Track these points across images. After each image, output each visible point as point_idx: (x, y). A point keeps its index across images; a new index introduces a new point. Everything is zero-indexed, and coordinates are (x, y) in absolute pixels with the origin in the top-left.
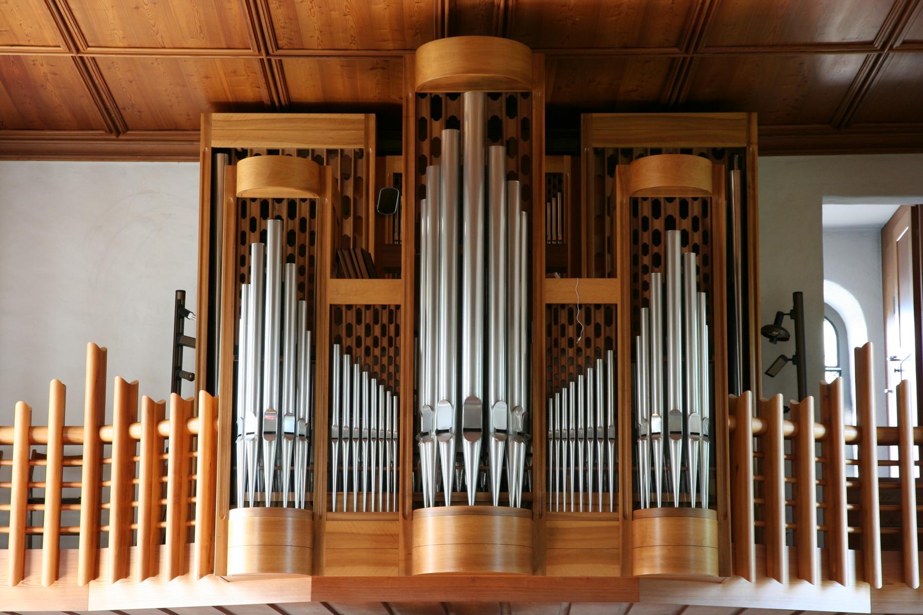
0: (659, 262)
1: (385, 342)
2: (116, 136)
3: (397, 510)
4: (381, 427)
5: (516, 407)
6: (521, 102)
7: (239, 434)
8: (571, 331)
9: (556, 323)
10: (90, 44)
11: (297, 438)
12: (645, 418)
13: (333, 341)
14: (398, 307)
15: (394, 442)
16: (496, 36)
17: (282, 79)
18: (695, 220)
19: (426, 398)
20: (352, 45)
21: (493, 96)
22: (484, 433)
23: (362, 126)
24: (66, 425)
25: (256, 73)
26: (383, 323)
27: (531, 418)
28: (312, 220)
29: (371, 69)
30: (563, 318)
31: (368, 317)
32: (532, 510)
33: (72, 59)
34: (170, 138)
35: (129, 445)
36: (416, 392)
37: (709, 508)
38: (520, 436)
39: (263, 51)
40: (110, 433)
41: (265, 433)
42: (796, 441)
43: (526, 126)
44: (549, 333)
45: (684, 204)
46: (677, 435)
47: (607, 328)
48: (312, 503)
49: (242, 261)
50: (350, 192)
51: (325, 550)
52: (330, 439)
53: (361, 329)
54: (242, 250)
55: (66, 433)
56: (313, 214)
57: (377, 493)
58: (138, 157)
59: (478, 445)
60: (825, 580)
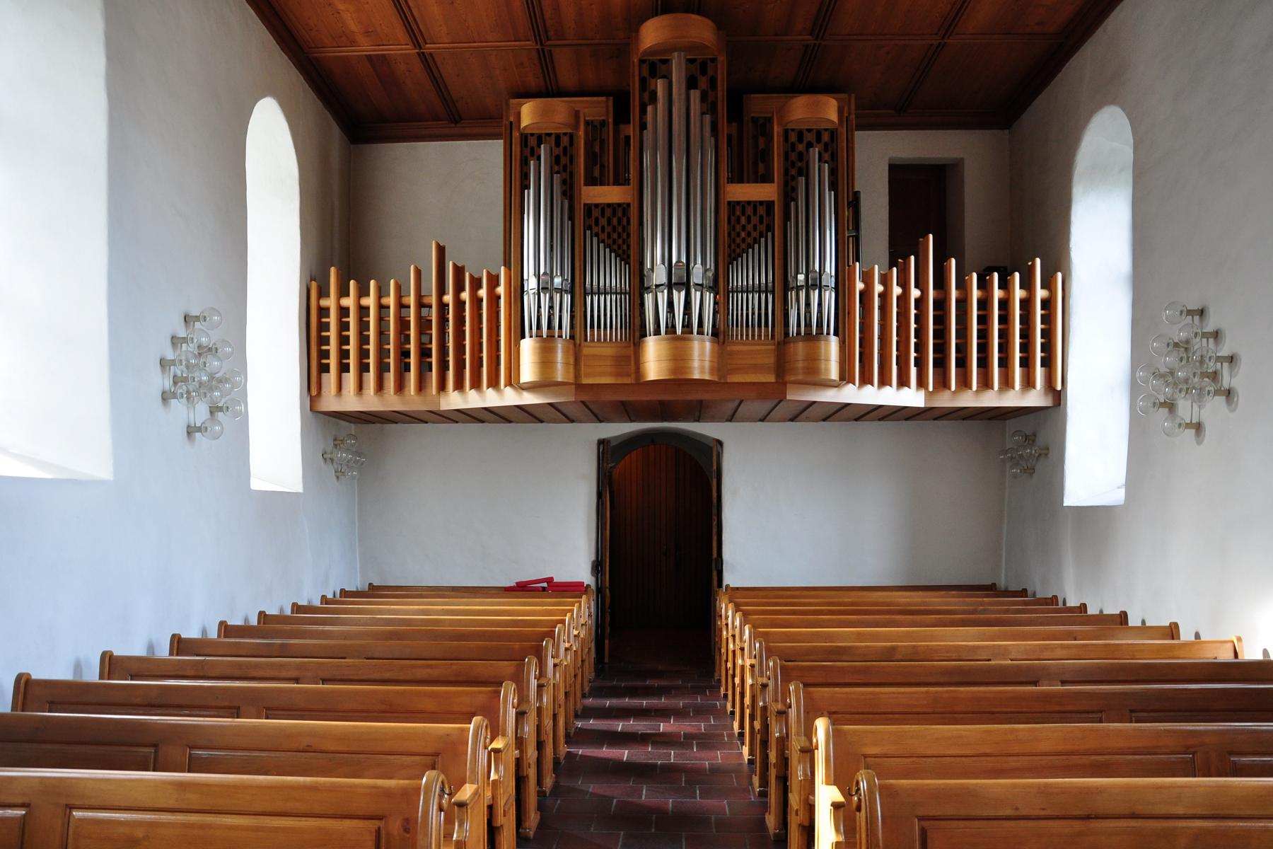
0: (805, 172)
1: (620, 229)
3: (630, 340)
9: (734, 214)
10: (428, 41)
14: (629, 205)
16: (693, 13)
18: (826, 144)
21: (691, 61)
22: (686, 285)
31: (608, 212)
35: (460, 304)
38: (711, 289)
39: (539, 43)
40: (449, 298)
42: (884, 296)
43: (713, 82)
44: (729, 222)
45: (819, 134)
50: (597, 149)
51: (583, 367)
52: (585, 294)
56: (571, 143)
59: (683, 293)
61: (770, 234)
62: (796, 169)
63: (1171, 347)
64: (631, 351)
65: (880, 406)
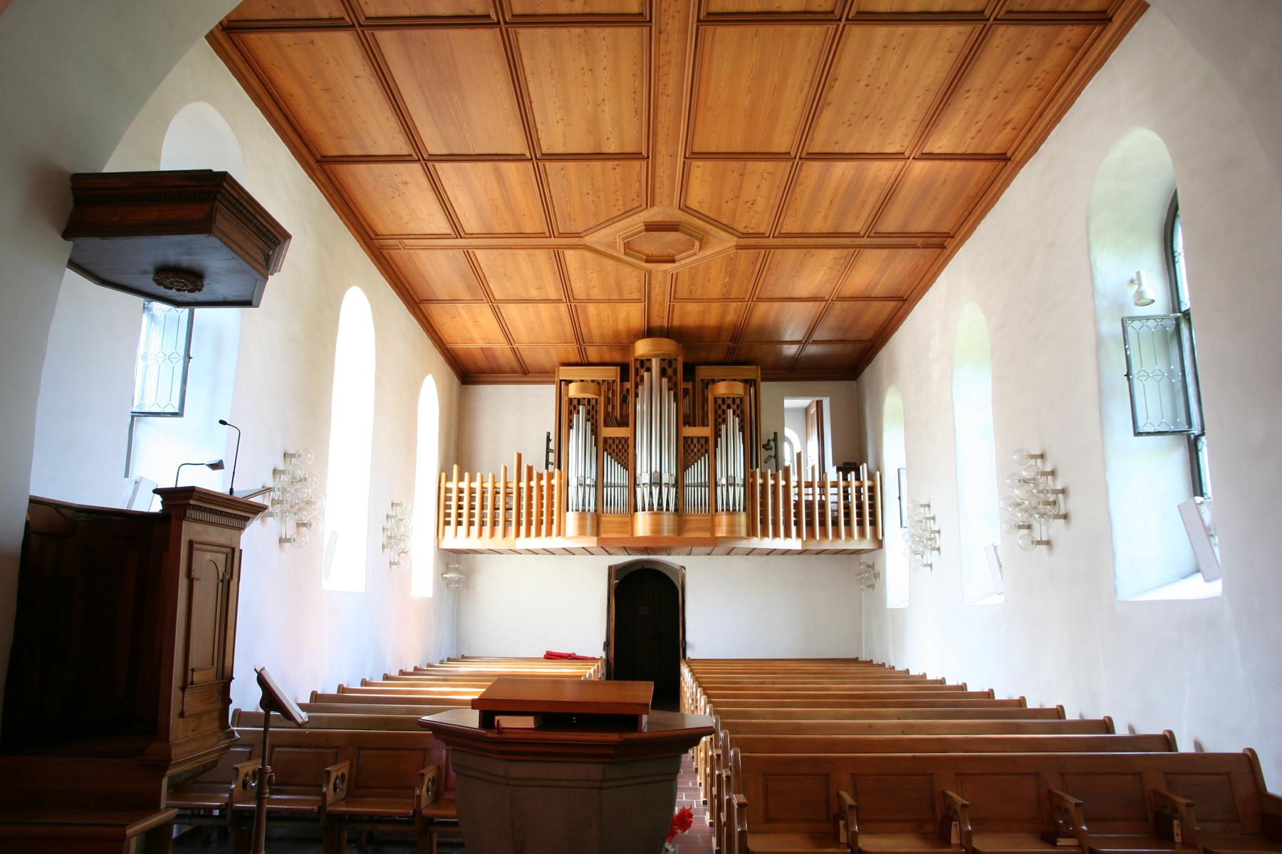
0: (725, 421)
1: (623, 451)
9: (687, 443)
14: (628, 438)
18: (738, 405)
31: (617, 442)
35: (530, 489)
36: (635, 469)
38: (673, 485)
40: (523, 484)
42: (775, 487)
43: (675, 371)
44: (684, 448)
45: (734, 400)
49: (571, 421)
50: (610, 396)
52: (603, 487)
59: (658, 489)
61: (707, 455)
62: (721, 420)
63: (1022, 483)
64: (628, 519)
65: (775, 549)
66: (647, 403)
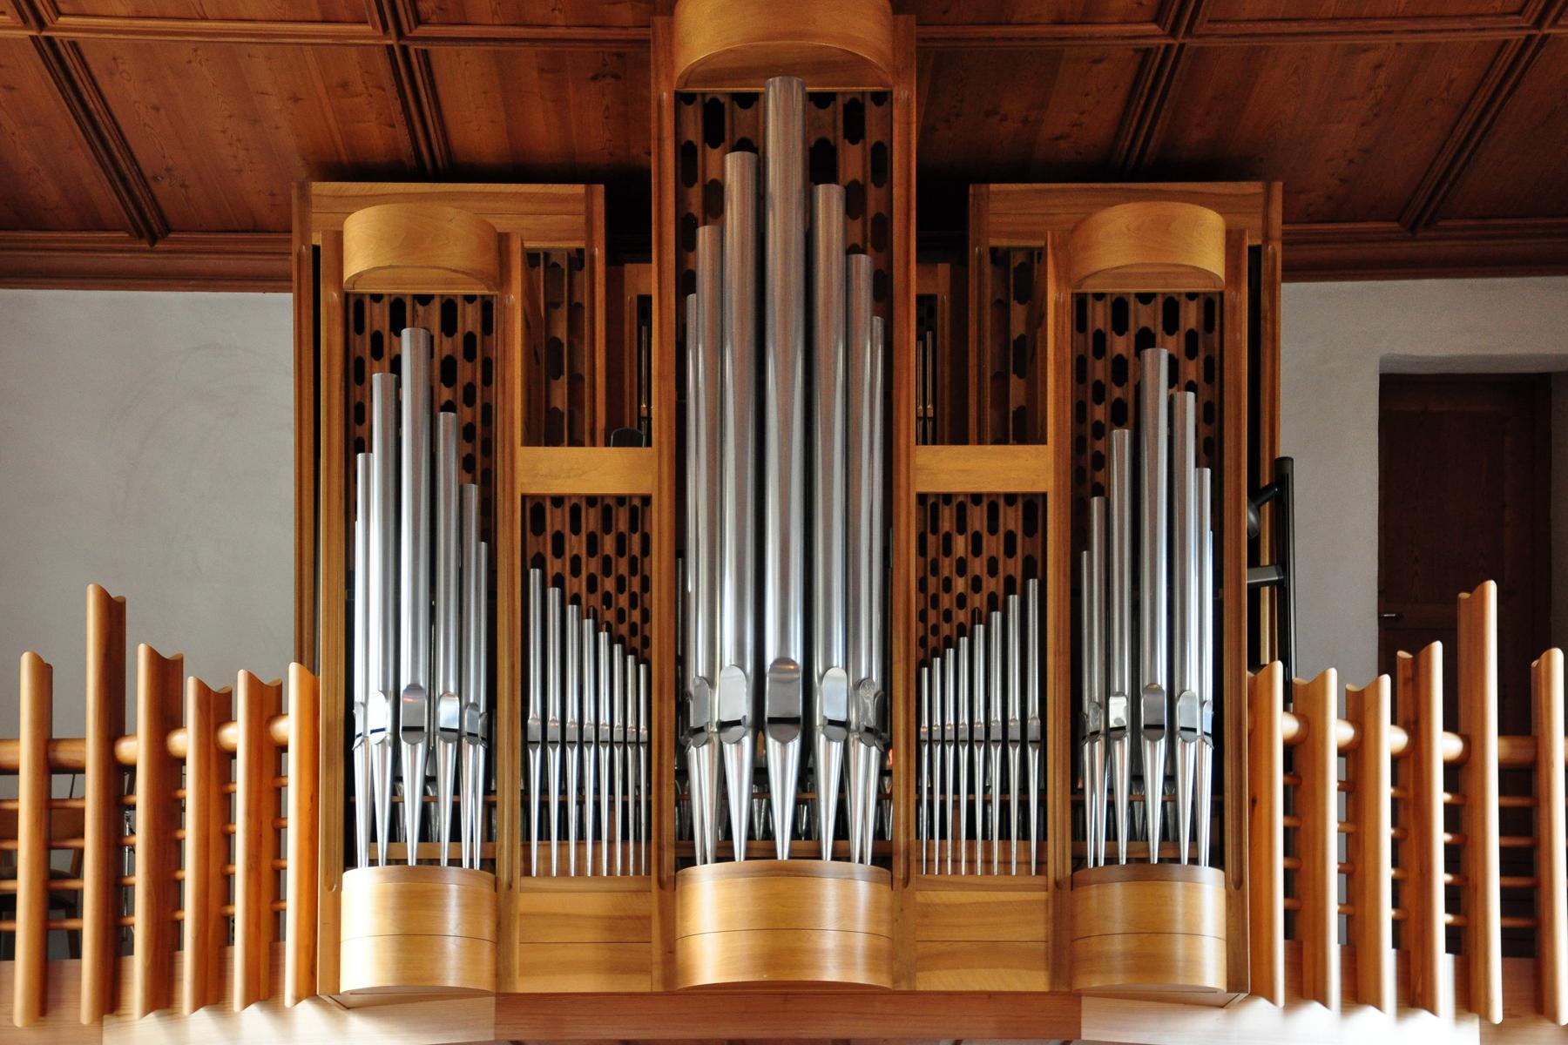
0: (1129, 414)
1: (623, 567)
2: (149, 244)
3: (648, 872)
4: (618, 722)
5: (864, 679)
6: (872, 112)
7: (357, 733)
8: (960, 545)
9: (935, 531)
10: (63, 7)
11: (464, 740)
12: (1097, 700)
13: (529, 563)
14: (646, 500)
15: (642, 748)
17: (432, 101)
18: (1191, 337)
19: (698, 665)
20: (557, 12)
22: (804, 725)
23: (582, 207)
24: (54, 737)
25: (384, 90)
26: (620, 530)
27: (888, 703)
28: (487, 337)
29: (595, 78)
30: (947, 522)
31: (590, 520)
32: (892, 871)
33: (32, 45)
34: (247, 247)
35: (168, 767)
36: (681, 661)
37: (1210, 865)
40: (135, 749)
41: (405, 729)
44: (922, 549)
45: (1171, 308)
46: (1157, 732)
47: (1027, 539)
48: (493, 861)
49: (357, 414)
50: (561, 332)
51: (517, 944)
52: (526, 744)
53: (580, 542)
54: (358, 393)
55: (54, 751)
56: (487, 325)
57: (611, 842)
58: (192, 282)
59: (794, 747)
60: (1403, 1006)
61: (1033, 585)
66: (740, 447)
